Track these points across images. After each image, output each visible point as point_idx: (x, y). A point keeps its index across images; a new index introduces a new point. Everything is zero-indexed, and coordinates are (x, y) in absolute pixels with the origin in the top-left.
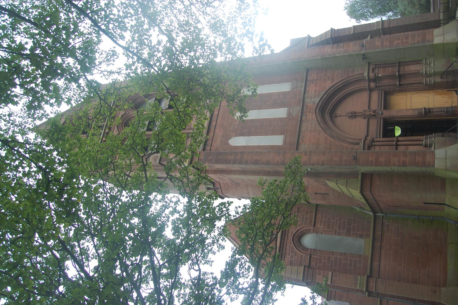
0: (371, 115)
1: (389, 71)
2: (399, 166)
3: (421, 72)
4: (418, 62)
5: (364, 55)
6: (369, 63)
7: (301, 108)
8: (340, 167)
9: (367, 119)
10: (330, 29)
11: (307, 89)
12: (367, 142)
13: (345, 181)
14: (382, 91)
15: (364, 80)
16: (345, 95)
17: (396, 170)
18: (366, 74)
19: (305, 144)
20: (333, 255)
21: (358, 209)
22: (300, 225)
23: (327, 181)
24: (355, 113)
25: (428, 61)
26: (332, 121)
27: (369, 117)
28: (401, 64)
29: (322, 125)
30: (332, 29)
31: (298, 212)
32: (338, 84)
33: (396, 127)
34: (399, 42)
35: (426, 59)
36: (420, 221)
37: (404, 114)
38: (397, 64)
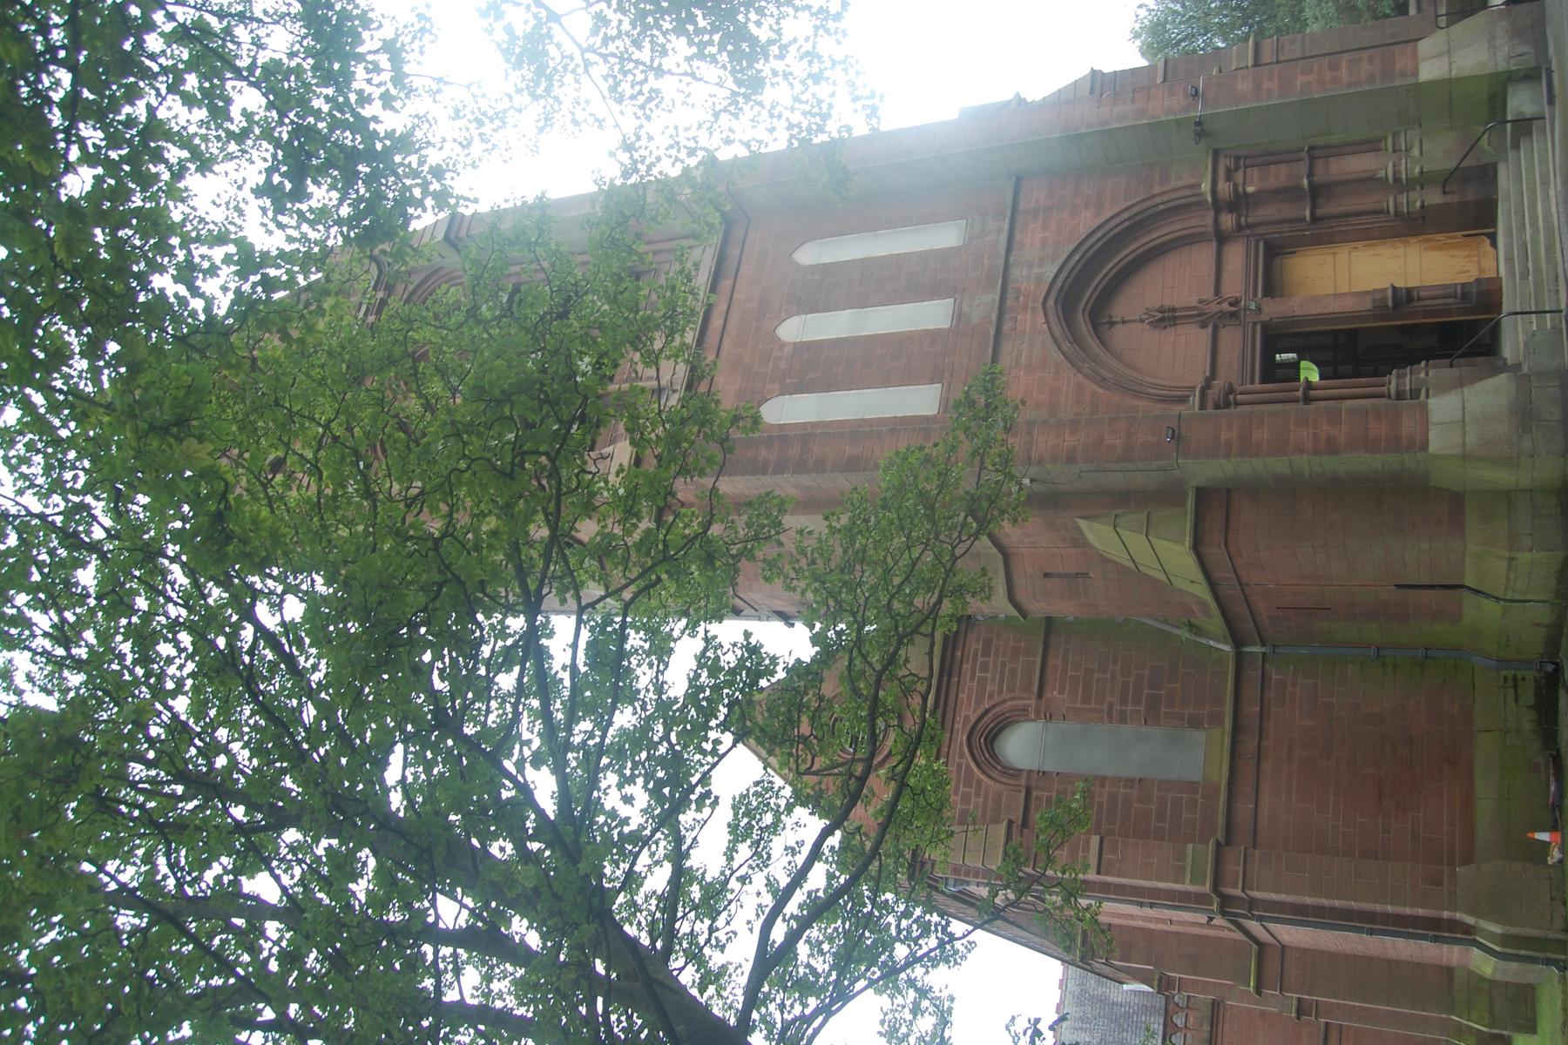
0: (1222, 314)
1: (1279, 175)
2: (1316, 452)
3: (1382, 174)
4: (1371, 145)
5: (1198, 124)
6: (1216, 154)
7: (997, 297)
8: (1129, 466)
9: (1210, 329)
10: (1087, 71)
11: (1018, 237)
13: (1144, 516)
14: (1257, 242)
15: (1200, 204)
16: (1139, 257)
18: (1206, 187)
20: (1102, 785)
21: (1185, 634)
22: (991, 696)
23: (1082, 523)
24: (1174, 310)
28: (1316, 153)
29: (1066, 346)
30: (1093, 71)
31: (986, 653)
32: (1116, 221)
34: (1310, 78)
36: (1384, 665)
37: (1329, 310)
38: (1304, 155)
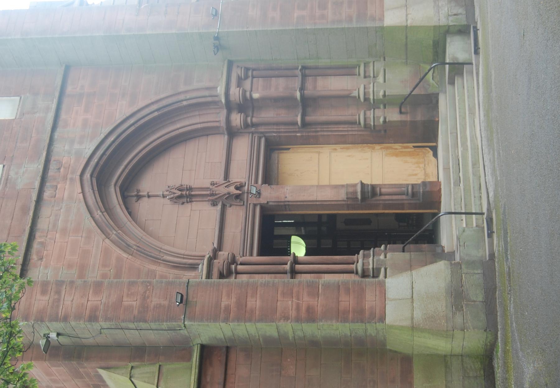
0: (229, 196)
1: (279, 87)
2: (298, 319)
3: (355, 94)
4: (348, 70)
5: (217, 38)
6: (230, 64)
7: (41, 167)
8: (143, 325)
9: (219, 207)
12: (218, 264)
13: (155, 368)
14: (260, 138)
15: (216, 103)
17: (291, 335)
18: (221, 90)
19: (46, 267)
23: (102, 372)
24: (190, 189)
25: (371, 68)
26: (127, 209)
27: (226, 200)
28: (307, 72)
29: (98, 214)
33: (294, 239)
35: (366, 65)
38: (298, 72)
